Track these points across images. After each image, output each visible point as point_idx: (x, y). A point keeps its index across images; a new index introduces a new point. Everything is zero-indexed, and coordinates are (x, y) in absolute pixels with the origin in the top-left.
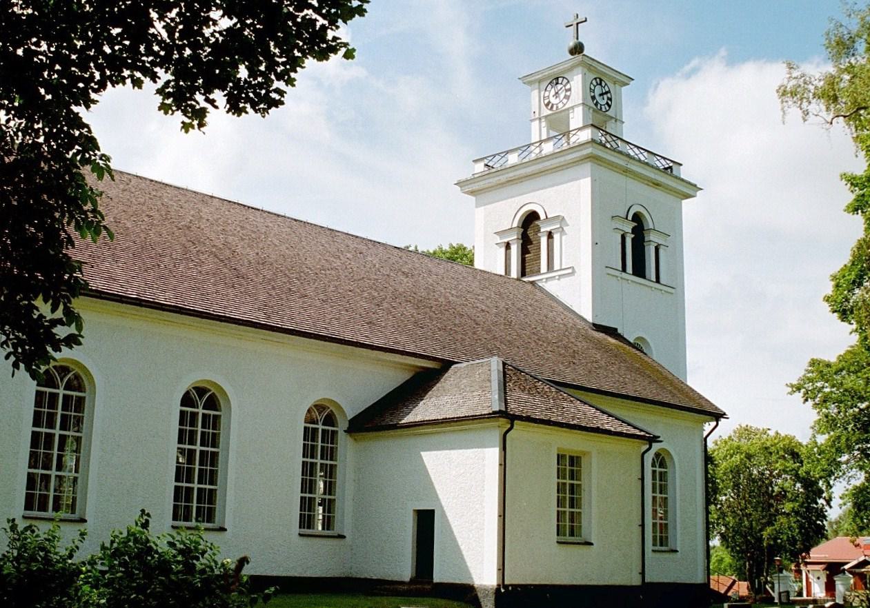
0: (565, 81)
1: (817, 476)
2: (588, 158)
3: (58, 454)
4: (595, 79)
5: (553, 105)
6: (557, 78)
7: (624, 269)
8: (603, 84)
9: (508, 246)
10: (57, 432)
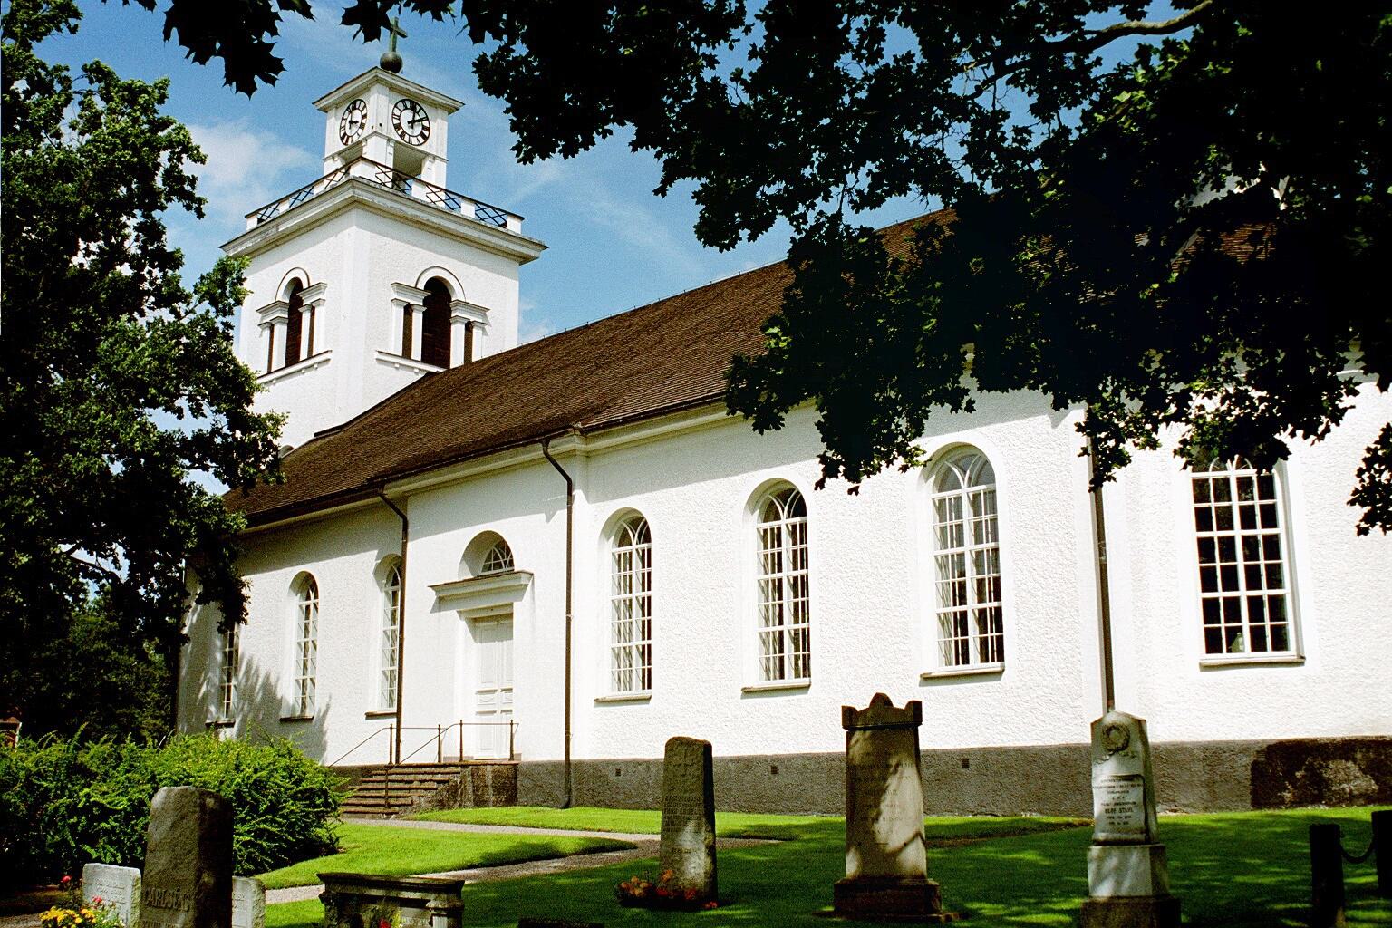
4: (403, 101)
7: (407, 353)
8: (418, 108)
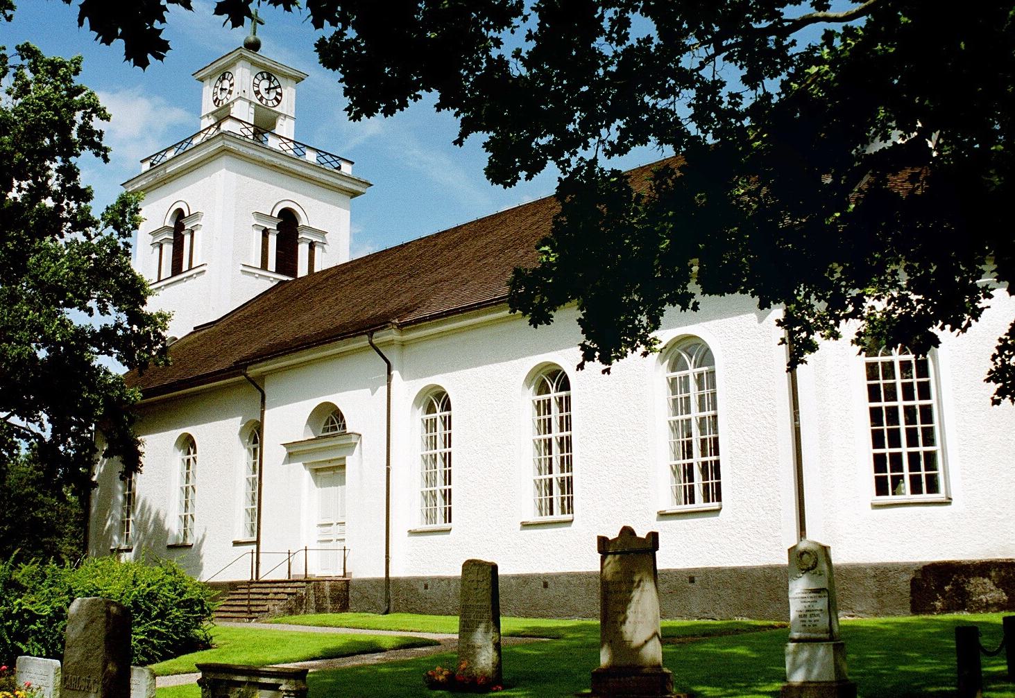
0: (230, 76)
1: (161, 562)
3: (898, 424)
4: (261, 73)
5: (220, 100)
7: (264, 266)
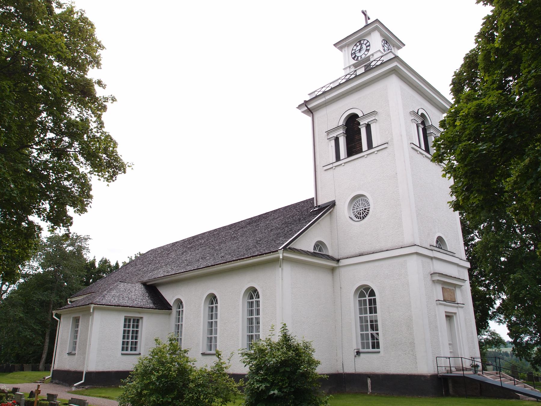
2: (393, 70)
5: (358, 57)
6: (360, 41)
9: (337, 139)
10: (131, 329)
